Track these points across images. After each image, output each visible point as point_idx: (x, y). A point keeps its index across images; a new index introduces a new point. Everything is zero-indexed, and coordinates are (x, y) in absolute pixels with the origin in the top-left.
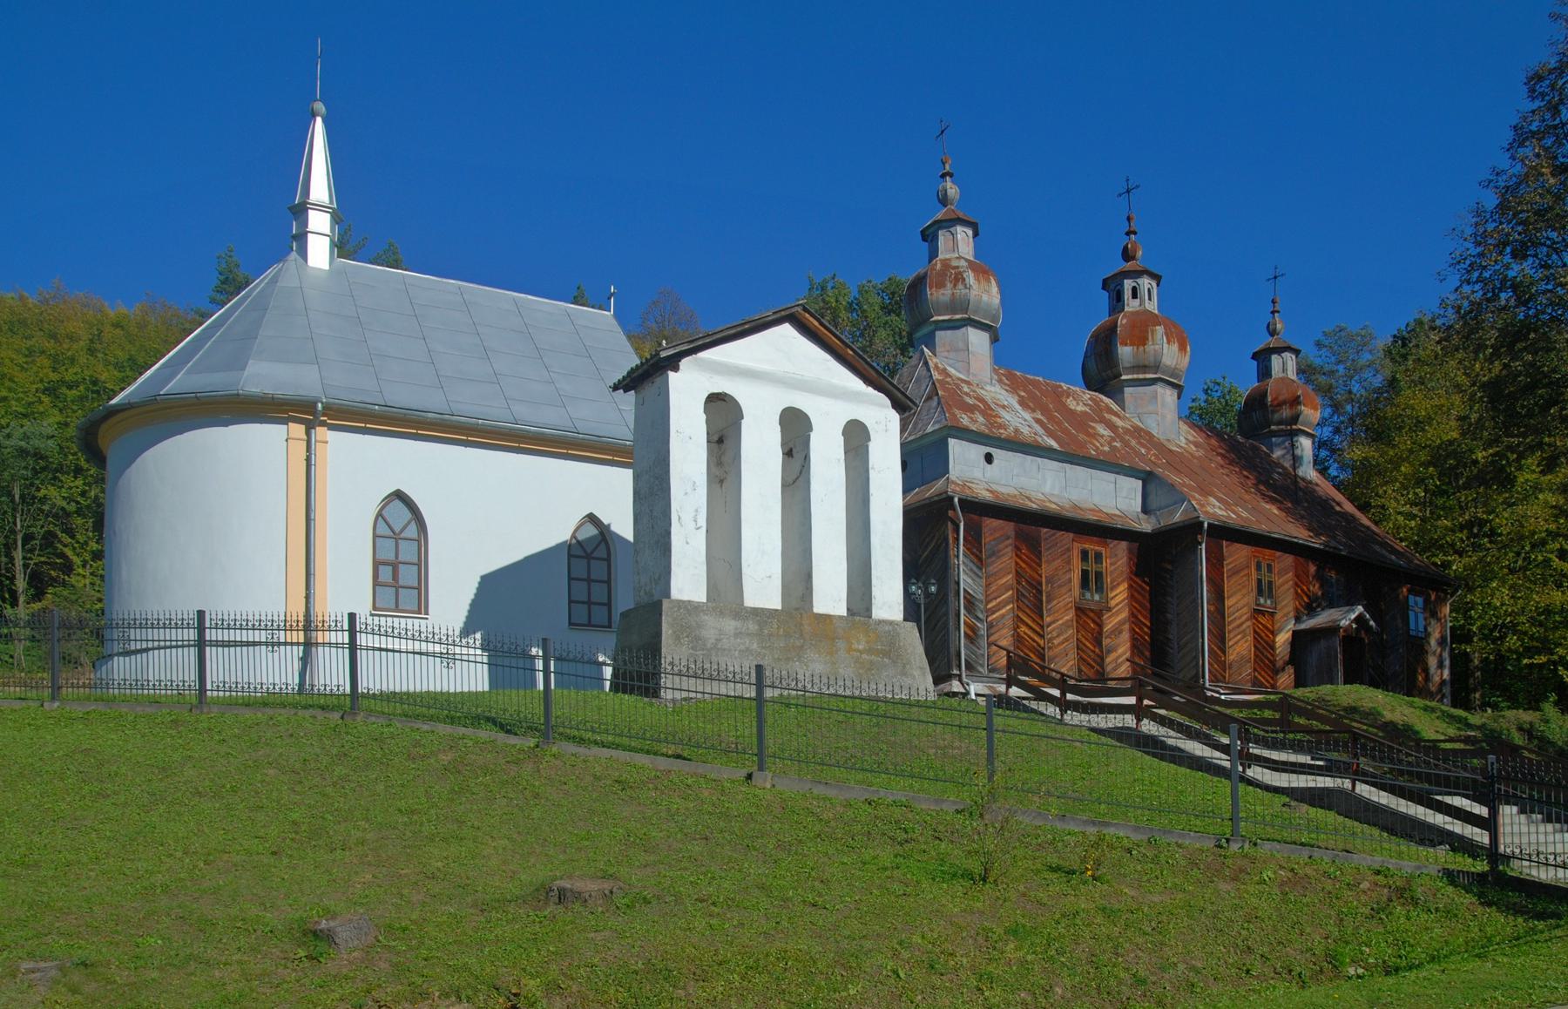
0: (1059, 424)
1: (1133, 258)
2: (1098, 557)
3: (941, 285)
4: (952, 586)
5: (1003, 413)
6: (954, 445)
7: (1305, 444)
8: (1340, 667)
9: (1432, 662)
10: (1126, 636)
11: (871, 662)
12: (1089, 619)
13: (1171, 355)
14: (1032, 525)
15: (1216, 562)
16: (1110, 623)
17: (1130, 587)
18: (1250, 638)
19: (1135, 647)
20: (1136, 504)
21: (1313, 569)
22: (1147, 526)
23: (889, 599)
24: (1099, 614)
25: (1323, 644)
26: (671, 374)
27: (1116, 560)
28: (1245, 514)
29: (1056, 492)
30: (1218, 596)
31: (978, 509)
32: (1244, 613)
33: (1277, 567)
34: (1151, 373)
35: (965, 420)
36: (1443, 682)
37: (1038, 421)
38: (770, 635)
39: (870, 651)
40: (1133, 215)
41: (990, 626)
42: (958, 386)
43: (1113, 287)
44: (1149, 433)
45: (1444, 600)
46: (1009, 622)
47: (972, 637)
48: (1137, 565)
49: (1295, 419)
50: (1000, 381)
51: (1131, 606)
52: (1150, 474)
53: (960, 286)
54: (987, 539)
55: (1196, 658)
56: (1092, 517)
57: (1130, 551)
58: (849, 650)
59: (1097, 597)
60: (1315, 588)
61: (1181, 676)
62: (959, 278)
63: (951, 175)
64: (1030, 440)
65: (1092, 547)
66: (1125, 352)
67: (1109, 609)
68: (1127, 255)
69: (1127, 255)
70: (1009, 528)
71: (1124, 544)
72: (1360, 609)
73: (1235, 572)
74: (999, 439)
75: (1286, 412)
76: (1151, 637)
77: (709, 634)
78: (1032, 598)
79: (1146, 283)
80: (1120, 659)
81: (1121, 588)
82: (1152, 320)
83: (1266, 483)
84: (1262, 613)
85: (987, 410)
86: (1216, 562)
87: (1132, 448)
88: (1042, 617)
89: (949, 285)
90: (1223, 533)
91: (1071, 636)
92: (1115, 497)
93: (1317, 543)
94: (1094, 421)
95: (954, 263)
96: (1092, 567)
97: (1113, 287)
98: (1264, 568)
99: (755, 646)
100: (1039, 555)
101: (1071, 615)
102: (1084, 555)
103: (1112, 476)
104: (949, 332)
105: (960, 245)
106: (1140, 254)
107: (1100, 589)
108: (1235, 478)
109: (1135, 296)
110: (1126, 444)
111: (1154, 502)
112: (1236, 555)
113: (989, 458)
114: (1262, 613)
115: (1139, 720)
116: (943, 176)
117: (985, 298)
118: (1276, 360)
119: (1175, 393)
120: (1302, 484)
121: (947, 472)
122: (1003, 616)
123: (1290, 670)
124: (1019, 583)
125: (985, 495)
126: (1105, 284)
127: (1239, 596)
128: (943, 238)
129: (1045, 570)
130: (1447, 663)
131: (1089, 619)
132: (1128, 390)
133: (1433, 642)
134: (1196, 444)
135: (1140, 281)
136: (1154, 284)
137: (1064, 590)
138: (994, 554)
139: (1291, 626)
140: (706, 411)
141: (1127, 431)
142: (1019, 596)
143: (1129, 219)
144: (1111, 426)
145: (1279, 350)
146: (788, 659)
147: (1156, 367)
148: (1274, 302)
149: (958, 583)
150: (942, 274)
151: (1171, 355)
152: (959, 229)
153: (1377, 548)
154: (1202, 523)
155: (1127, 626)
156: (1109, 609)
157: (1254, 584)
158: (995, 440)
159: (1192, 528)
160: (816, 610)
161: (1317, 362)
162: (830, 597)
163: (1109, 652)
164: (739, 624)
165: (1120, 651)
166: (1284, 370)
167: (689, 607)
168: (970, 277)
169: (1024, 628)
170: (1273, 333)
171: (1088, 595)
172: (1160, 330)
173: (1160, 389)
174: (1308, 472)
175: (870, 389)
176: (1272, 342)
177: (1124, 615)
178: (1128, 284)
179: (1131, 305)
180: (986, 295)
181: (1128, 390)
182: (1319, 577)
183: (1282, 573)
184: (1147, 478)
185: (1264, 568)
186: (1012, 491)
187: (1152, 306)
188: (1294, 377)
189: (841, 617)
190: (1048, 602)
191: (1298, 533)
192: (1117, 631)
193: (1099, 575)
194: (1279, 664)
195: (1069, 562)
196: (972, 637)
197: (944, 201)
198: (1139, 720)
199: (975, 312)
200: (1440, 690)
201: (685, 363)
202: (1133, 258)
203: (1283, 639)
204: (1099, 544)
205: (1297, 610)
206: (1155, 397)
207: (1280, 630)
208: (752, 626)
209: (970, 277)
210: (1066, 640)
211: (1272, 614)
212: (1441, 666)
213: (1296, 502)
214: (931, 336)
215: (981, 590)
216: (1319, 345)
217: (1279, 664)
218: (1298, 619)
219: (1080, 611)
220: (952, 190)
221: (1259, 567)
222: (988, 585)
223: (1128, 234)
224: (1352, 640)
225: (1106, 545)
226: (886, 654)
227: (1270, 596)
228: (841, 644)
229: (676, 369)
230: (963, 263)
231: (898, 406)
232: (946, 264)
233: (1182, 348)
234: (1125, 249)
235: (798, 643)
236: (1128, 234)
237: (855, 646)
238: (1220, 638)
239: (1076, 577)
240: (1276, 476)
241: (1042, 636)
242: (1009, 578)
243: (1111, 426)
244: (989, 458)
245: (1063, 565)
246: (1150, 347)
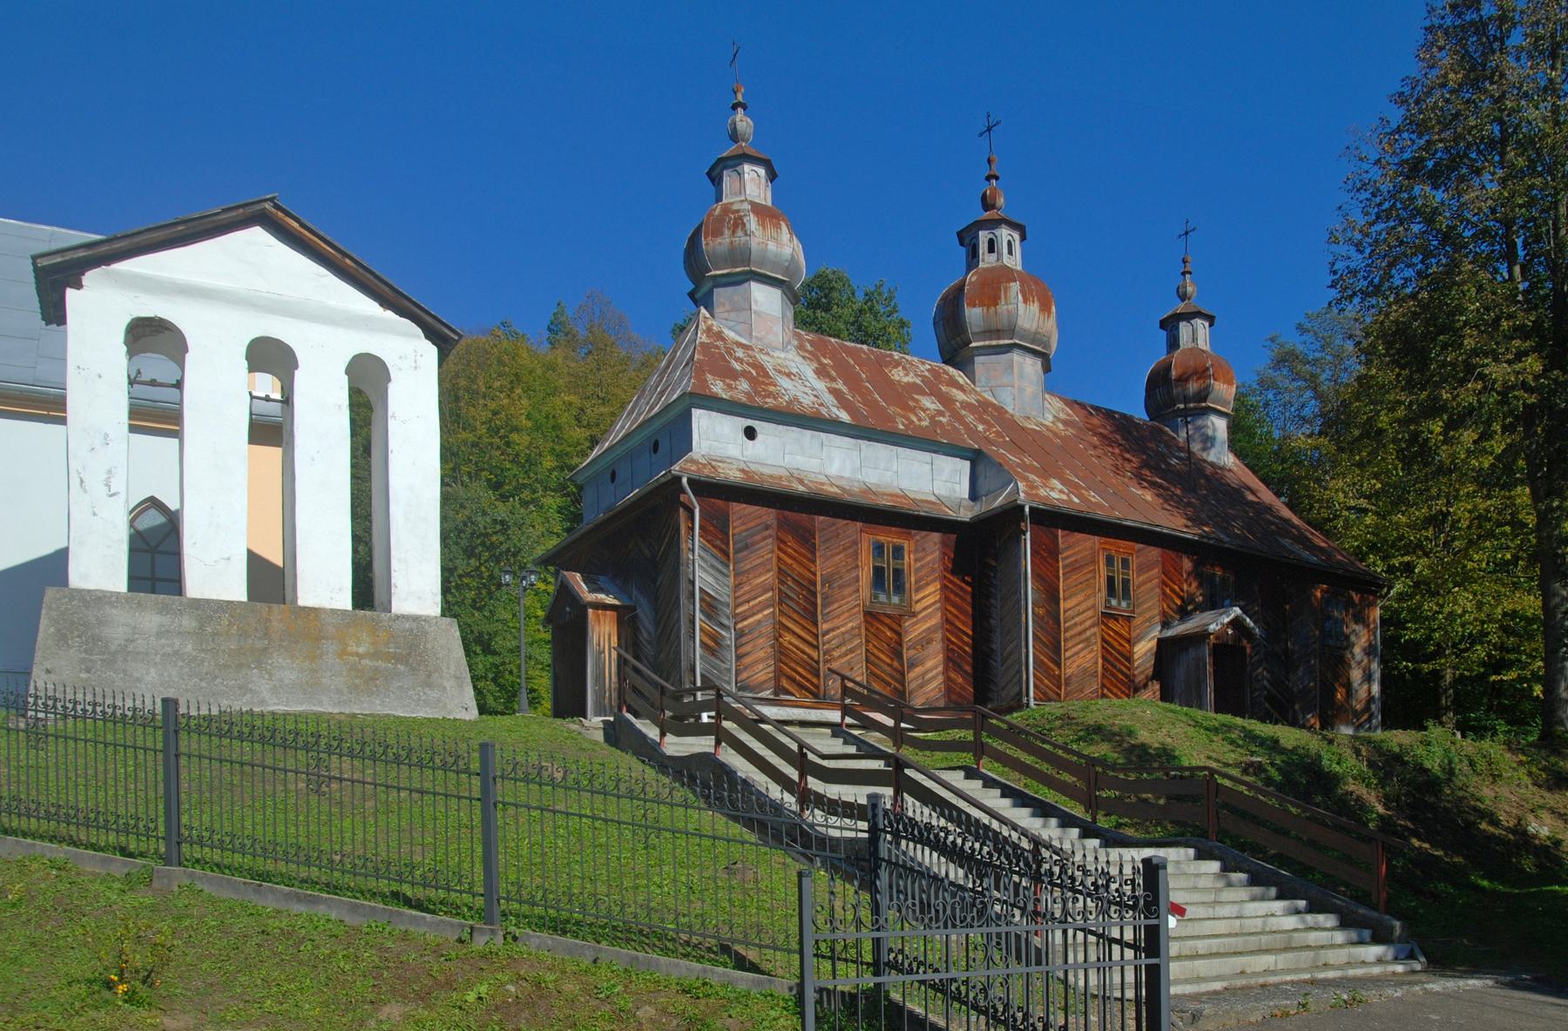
0: (864, 394)
1: (993, 207)
2: (898, 552)
3: (718, 233)
4: (683, 584)
5: (785, 383)
6: (702, 420)
7: (1219, 426)
8: (1210, 682)
9: (1356, 675)
10: (937, 646)
11: (376, 669)
12: (884, 628)
13: (1028, 316)
14: (801, 511)
15: (1047, 556)
16: (914, 631)
17: (944, 587)
18: (1097, 647)
19: (951, 661)
20: (963, 490)
21: (1187, 564)
22: (965, 515)
23: (416, 582)
24: (898, 619)
25: (1192, 653)
26: (71, 293)
27: (925, 558)
28: (1094, 497)
29: (847, 474)
30: (1051, 596)
31: (722, 494)
32: (1089, 618)
33: (1134, 563)
34: (1005, 340)
35: (718, 388)
36: (1371, 699)
37: (835, 393)
38: (215, 634)
39: (376, 655)
40: (994, 157)
41: (740, 634)
42: (729, 351)
43: (967, 238)
44: (1000, 410)
45: (1372, 604)
46: (767, 628)
47: (714, 647)
48: (954, 562)
49: (1203, 395)
50: (801, 347)
51: (945, 610)
52: (978, 453)
53: (740, 233)
54: (736, 528)
55: (1019, 672)
56: (885, 502)
57: (944, 544)
58: (343, 653)
59: (895, 600)
60: (1191, 587)
61: (1004, 694)
62: (739, 223)
63: (745, 107)
64: (808, 411)
65: (889, 538)
66: (974, 315)
67: (914, 615)
68: (987, 204)
69: (987, 204)
70: (769, 515)
71: (936, 537)
72: (1237, 611)
73: (1073, 568)
74: (761, 409)
75: (1193, 387)
76: (974, 648)
77: (116, 633)
78: (802, 601)
79: (1004, 234)
80: (929, 678)
81: (931, 589)
82: (1007, 274)
83: (1156, 469)
84: (1115, 618)
85: (760, 377)
86: (1047, 556)
87: (965, 425)
88: (816, 624)
89: (727, 232)
90: (1051, 519)
91: (860, 645)
92: (938, 482)
93: (1191, 533)
94: (923, 393)
95: (735, 207)
96: (889, 564)
97: (967, 238)
98: (1118, 564)
99: (189, 648)
100: (813, 550)
101: (857, 621)
102: (879, 549)
103: (927, 456)
104: (730, 289)
105: (752, 184)
106: (1001, 201)
107: (899, 588)
108: (1108, 462)
109: (991, 249)
110: (961, 419)
111: (984, 486)
112: (1086, 544)
113: (750, 433)
114: (1115, 618)
115: (663, 735)
116: (734, 107)
117: (772, 246)
118: (1184, 329)
119: (1039, 362)
120: (1209, 470)
121: (690, 449)
122: (759, 621)
123: (1156, 686)
124: (782, 582)
125: (732, 475)
126: (960, 234)
127: (1080, 597)
128: (728, 179)
129: (821, 568)
130: (1377, 675)
131: (884, 628)
132: (978, 359)
133: (1357, 650)
134: (1065, 423)
135: (997, 232)
136: (1016, 236)
137: (846, 592)
138: (747, 547)
139: (1156, 632)
140: (126, 343)
141: (967, 406)
142: (783, 598)
143: (989, 161)
144: (946, 401)
145: (1188, 317)
146: (240, 666)
147: (1011, 331)
148: (1184, 262)
149: (693, 583)
150: (720, 220)
151: (1028, 316)
152: (747, 168)
153: (1286, 542)
154: (1022, 507)
155: (939, 636)
156: (914, 615)
157: (1103, 583)
158: (760, 410)
159: (1013, 512)
160: (301, 602)
161: (1300, 348)
162: (324, 582)
163: (912, 666)
164: (166, 620)
165: (929, 664)
166: (1194, 339)
167: (99, 599)
168: (752, 222)
169: (788, 637)
170: (1183, 297)
171: (882, 598)
172: (1015, 287)
173: (1016, 356)
174: (1223, 457)
175: (390, 314)
176: (1180, 307)
177: (936, 620)
178: (984, 236)
179: (987, 260)
180: (781, 245)
181: (978, 359)
182: (1197, 574)
183: (1142, 569)
184: (976, 458)
185: (1118, 564)
186: (776, 472)
187: (1015, 262)
188: (1207, 348)
189: (240, 603)
190: (824, 606)
191: (1173, 522)
192: (925, 641)
193: (898, 573)
194: (1140, 679)
195: (856, 555)
196: (714, 647)
197: (734, 136)
198: (663, 735)
199: (761, 265)
200: (1367, 708)
201: (89, 277)
202: (993, 207)
203: (1144, 649)
204: (899, 535)
205: (1164, 614)
206: (1011, 367)
207: (1139, 638)
208: (188, 623)
209: (752, 222)
210: (851, 651)
211: (1129, 619)
212: (1368, 678)
213: (1190, 488)
214: (711, 292)
215: (726, 590)
216: (1300, 328)
217: (1140, 679)
218: (1166, 625)
219: (871, 616)
220: (743, 122)
221: (1110, 561)
222: (737, 586)
223: (988, 178)
224: (1227, 652)
225: (908, 537)
226: (398, 658)
227: (1126, 594)
228: (331, 647)
229: (79, 286)
230: (746, 206)
231: (432, 334)
232: (727, 210)
233: (1045, 308)
234: (984, 197)
235: (259, 645)
236: (988, 178)
237: (353, 648)
238: (1053, 646)
239: (866, 575)
240: (1174, 461)
241: (816, 647)
242: (768, 577)
243: (946, 401)
244: (750, 433)
245: (848, 560)
246: (1003, 308)
